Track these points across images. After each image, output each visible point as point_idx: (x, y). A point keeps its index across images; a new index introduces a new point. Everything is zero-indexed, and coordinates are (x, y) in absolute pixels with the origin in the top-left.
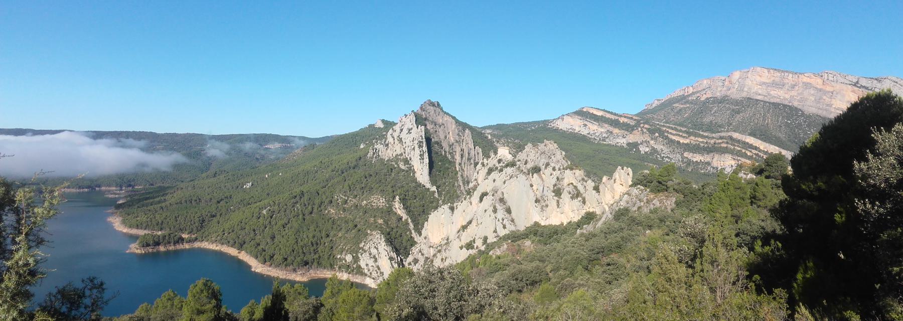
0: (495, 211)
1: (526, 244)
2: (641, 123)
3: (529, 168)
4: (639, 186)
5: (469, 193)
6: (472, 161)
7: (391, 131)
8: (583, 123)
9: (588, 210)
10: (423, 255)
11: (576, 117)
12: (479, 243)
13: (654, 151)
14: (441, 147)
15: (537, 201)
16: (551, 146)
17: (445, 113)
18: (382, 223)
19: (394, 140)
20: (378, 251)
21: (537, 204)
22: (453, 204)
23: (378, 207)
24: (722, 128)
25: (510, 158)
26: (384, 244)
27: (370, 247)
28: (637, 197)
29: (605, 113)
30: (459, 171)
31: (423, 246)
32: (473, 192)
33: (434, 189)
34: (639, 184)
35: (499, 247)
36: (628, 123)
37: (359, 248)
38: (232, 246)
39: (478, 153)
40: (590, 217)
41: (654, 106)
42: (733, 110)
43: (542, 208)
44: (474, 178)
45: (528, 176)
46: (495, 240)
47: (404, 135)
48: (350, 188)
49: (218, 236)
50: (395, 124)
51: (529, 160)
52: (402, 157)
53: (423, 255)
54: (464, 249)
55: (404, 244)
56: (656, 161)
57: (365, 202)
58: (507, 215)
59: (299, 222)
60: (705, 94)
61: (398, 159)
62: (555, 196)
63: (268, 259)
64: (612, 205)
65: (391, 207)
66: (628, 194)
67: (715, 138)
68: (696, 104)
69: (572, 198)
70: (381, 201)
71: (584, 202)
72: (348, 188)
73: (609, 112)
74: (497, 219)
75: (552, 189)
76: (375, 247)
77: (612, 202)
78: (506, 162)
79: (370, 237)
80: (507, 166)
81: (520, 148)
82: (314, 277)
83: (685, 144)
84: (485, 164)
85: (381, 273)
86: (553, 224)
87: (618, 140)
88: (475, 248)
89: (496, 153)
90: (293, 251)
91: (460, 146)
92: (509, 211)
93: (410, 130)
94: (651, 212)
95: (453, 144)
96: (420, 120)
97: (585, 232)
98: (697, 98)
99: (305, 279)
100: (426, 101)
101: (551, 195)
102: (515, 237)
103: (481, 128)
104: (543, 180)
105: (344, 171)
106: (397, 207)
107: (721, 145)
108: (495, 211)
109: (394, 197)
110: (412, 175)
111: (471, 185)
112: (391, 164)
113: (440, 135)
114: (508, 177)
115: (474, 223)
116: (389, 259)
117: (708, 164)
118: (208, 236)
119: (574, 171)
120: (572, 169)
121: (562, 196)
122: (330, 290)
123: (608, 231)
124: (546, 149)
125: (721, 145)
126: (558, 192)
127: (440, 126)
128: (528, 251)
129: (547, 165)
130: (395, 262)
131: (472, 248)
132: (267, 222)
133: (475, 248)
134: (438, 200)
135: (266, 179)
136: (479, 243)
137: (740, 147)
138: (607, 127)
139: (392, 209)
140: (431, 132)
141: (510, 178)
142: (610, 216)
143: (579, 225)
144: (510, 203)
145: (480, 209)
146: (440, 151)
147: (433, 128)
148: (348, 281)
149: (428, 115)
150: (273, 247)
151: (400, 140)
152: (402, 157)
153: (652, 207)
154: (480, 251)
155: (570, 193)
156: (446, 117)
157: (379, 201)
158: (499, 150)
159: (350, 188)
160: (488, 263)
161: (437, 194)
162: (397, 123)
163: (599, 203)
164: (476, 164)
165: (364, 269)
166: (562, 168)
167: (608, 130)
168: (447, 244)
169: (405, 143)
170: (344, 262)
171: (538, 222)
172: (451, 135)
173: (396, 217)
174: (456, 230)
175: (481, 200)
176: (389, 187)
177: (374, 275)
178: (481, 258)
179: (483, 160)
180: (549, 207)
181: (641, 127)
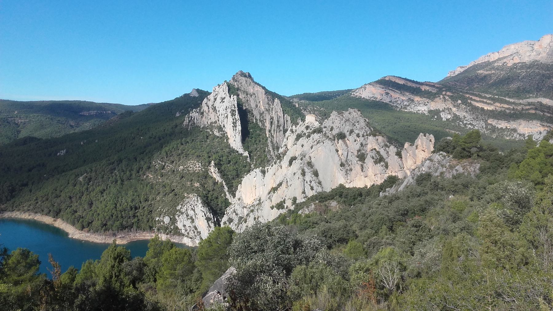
0: (303, 174)
1: (332, 205)
2: (444, 91)
3: (334, 134)
4: (441, 152)
5: (280, 157)
6: (281, 128)
7: (205, 100)
8: (384, 92)
9: (390, 174)
10: (237, 214)
11: (378, 85)
12: (289, 204)
13: (456, 118)
14: (252, 115)
15: (342, 165)
16: (354, 114)
17: (256, 83)
18: (199, 186)
19: (209, 108)
20: (195, 212)
22: (264, 168)
23: (195, 172)
24: (531, 94)
25: (317, 124)
26: (201, 205)
27: (187, 209)
28: (439, 163)
29: (407, 81)
30: (269, 137)
31: (237, 207)
32: (283, 157)
33: (246, 154)
34: (442, 150)
35: (308, 207)
36: (430, 91)
37: (177, 210)
38: (46, 215)
39: (287, 121)
40: (392, 181)
41: (457, 73)
42: (543, 75)
43: (346, 172)
44: (284, 144)
45: (333, 142)
46: (304, 200)
47: (217, 104)
48: (167, 154)
49: (30, 205)
50: (210, 94)
51: (334, 127)
52: (216, 125)
53: (237, 214)
54: (275, 209)
55: (220, 205)
56: (459, 128)
57: (181, 167)
58: (315, 178)
59: (118, 188)
60: (513, 59)
61: (212, 126)
62: (359, 161)
63: (85, 226)
64: (414, 170)
65: (207, 171)
66: (430, 159)
67: (523, 104)
68: (502, 70)
69: (376, 163)
71: (387, 166)
72: (165, 154)
73: (410, 81)
74: (306, 182)
75: (356, 154)
76: (192, 209)
77: (413, 167)
78: (313, 129)
79: (187, 200)
80: (314, 132)
81: (324, 116)
82: (133, 239)
83: (490, 111)
84: (294, 130)
85: (198, 232)
86: (358, 187)
87: (419, 108)
88: (285, 208)
89: (303, 120)
90: (112, 216)
91: (269, 114)
92: (316, 174)
93: (223, 99)
94: (454, 177)
95: (263, 112)
96: (232, 90)
97: (387, 194)
98: (503, 64)
99: (124, 242)
100: (238, 72)
101: (355, 160)
102: (322, 198)
103: (289, 97)
104: (347, 146)
105: (161, 138)
106: (212, 171)
107: (529, 111)
108: (303, 174)
109: (210, 163)
110: (225, 141)
111: (281, 150)
112: (207, 132)
113: (252, 104)
114: (315, 143)
115: (284, 185)
116: (206, 219)
117: (515, 130)
118: (20, 205)
119: (377, 137)
120: (375, 135)
121: (365, 161)
122: (153, 250)
123: (411, 194)
124: (351, 117)
125: (529, 111)
126: (362, 157)
127: (251, 96)
128: (334, 210)
129: (351, 132)
130: (212, 222)
131: (283, 208)
132: (84, 189)
133: (285, 208)
134: (250, 165)
135: (82, 146)
136: (289, 204)
137: (550, 113)
138: (408, 95)
139: (208, 174)
140: (243, 101)
141: (317, 143)
142: (411, 180)
143: (382, 188)
144: (318, 166)
145: (290, 172)
146: (252, 119)
147: (245, 97)
148: (168, 242)
149: (240, 86)
150: (91, 213)
151: (214, 109)
152: (216, 125)
153: (455, 173)
154: (290, 210)
155: (373, 158)
156: (257, 87)
157: (196, 166)
158: (306, 117)
159: (167, 154)
160: (298, 221)
161: (249, 159)
162: (211, 93)
163: (401, 168)
164: (285, 131)
165: (181, 230)
166: (365, 134)
167: (409, 98)
168: (260, 204)
169: (219, 111)
170: (162, 223)
171: (343, 185)
172: (261, 104)
173: (211, 180)
174: (267, 192)
175: (290, 163)
176: (204, 152)
177: (191, 234)
178: (291, 217)
179: (292, 127)
180: (353, 171)
181: (442, 95)
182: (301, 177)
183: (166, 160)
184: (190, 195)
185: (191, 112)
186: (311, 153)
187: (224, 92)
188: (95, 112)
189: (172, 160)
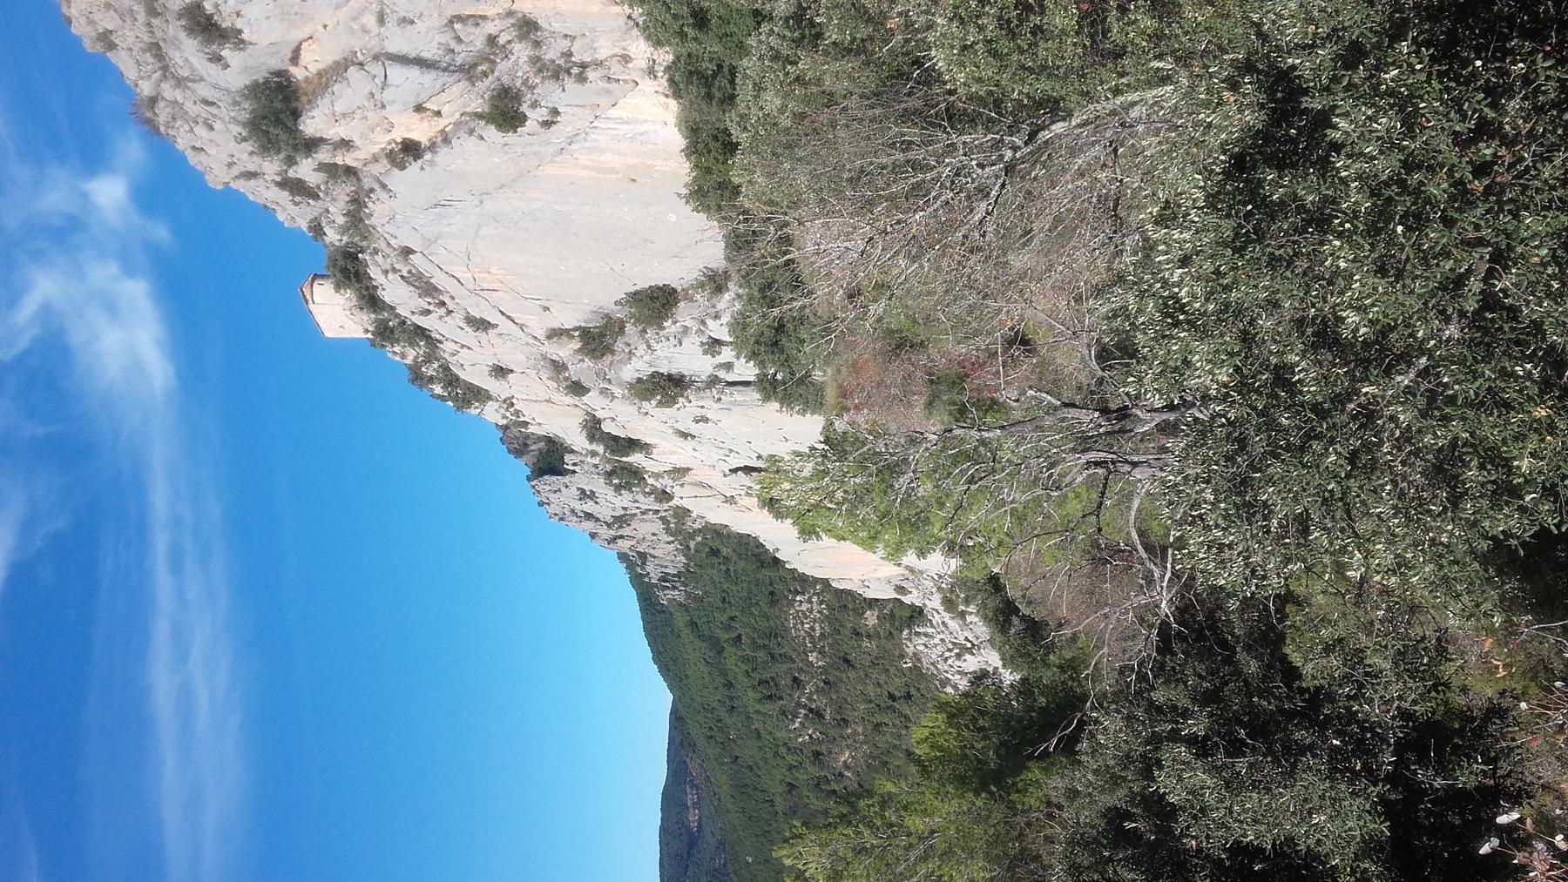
18: (876, 614)
21: (534, 116)
27: (959, 672)
43: (556, 73)
58: (685, 314)
70: (805, 607)
76: (958, 656)
93: (584, 495)
104: (338, 70)
169: (625, 509)
182: (684, 412)
183: (791, 701)
184: (907, 650)
185: (647, 580)
186: (521, 327)
187: (560, 490)
188: (688, 790)
189: (789, 681)
